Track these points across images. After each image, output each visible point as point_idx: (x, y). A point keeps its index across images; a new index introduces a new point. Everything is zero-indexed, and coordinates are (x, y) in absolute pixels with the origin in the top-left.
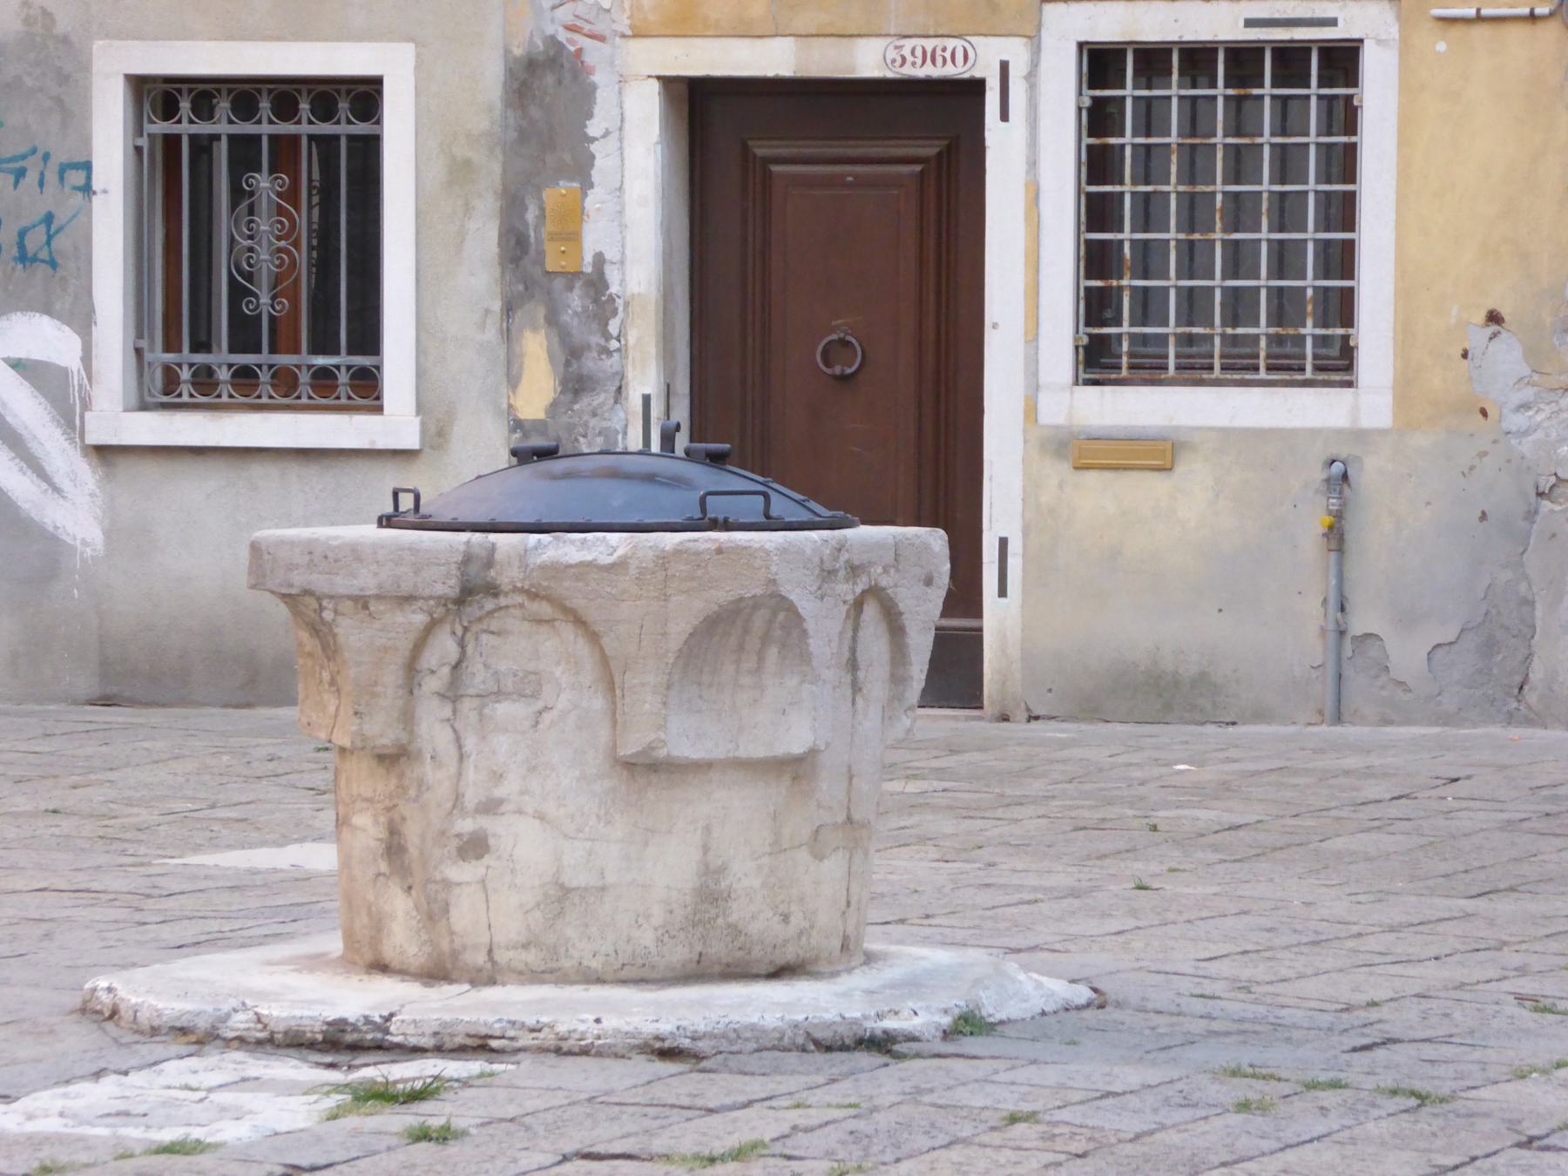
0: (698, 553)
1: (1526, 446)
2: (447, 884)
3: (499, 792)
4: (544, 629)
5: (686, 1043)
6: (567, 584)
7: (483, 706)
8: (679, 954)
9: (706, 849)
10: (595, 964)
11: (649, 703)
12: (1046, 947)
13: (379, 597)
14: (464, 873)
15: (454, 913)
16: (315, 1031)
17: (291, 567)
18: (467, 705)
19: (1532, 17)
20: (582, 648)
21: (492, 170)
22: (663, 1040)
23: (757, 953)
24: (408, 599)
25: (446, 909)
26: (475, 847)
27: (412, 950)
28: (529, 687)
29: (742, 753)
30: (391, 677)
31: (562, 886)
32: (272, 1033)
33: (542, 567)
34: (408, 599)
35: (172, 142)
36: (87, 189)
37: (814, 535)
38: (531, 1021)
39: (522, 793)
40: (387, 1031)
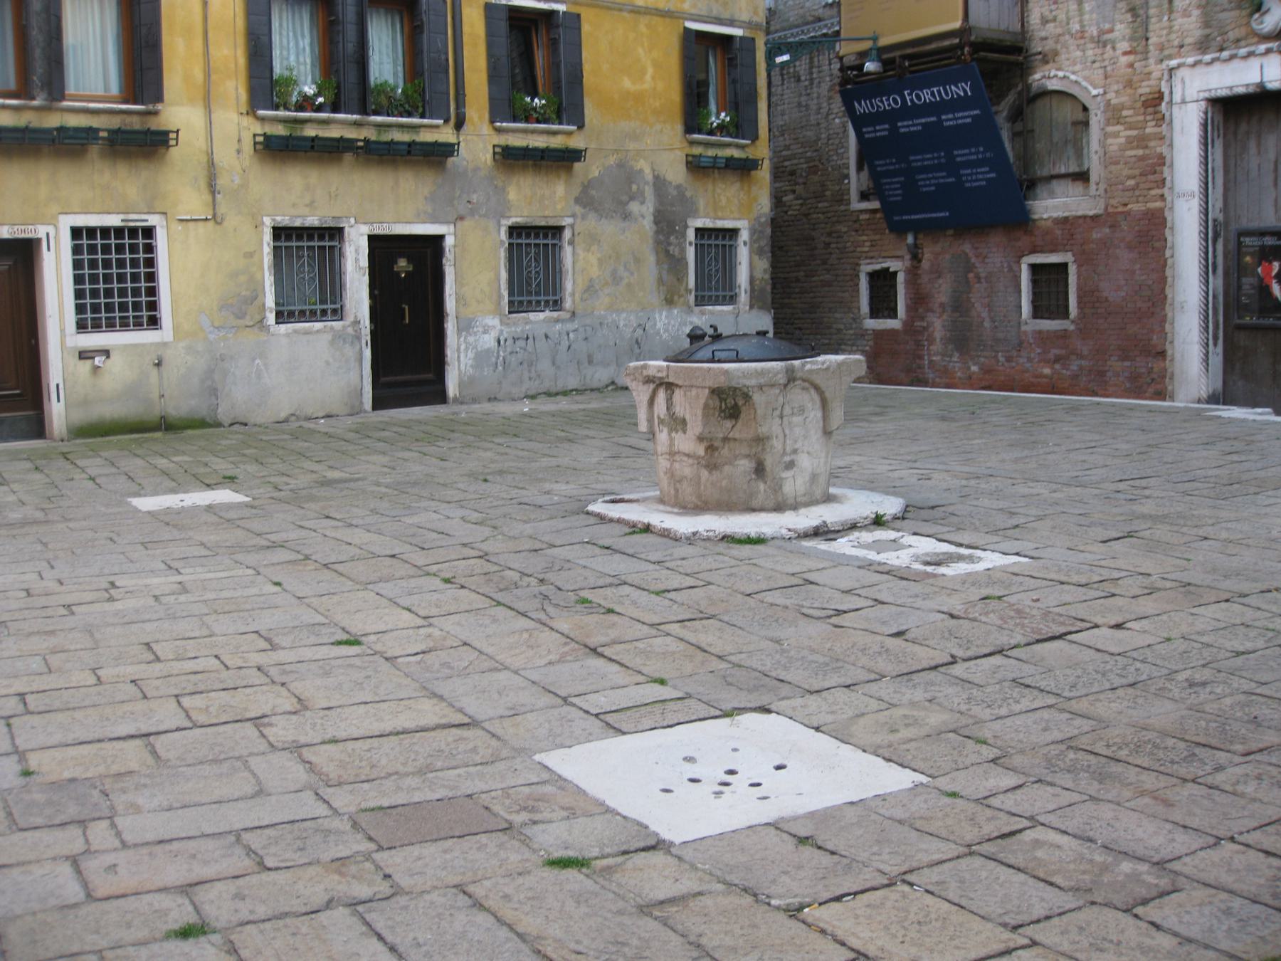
2: (782, 479)
3: (796, 447)
12: (336, 523)
15: (784, 488)
17: (739, 377)
19: (206, 219)
25: (781, 487)
37: (774, 363)
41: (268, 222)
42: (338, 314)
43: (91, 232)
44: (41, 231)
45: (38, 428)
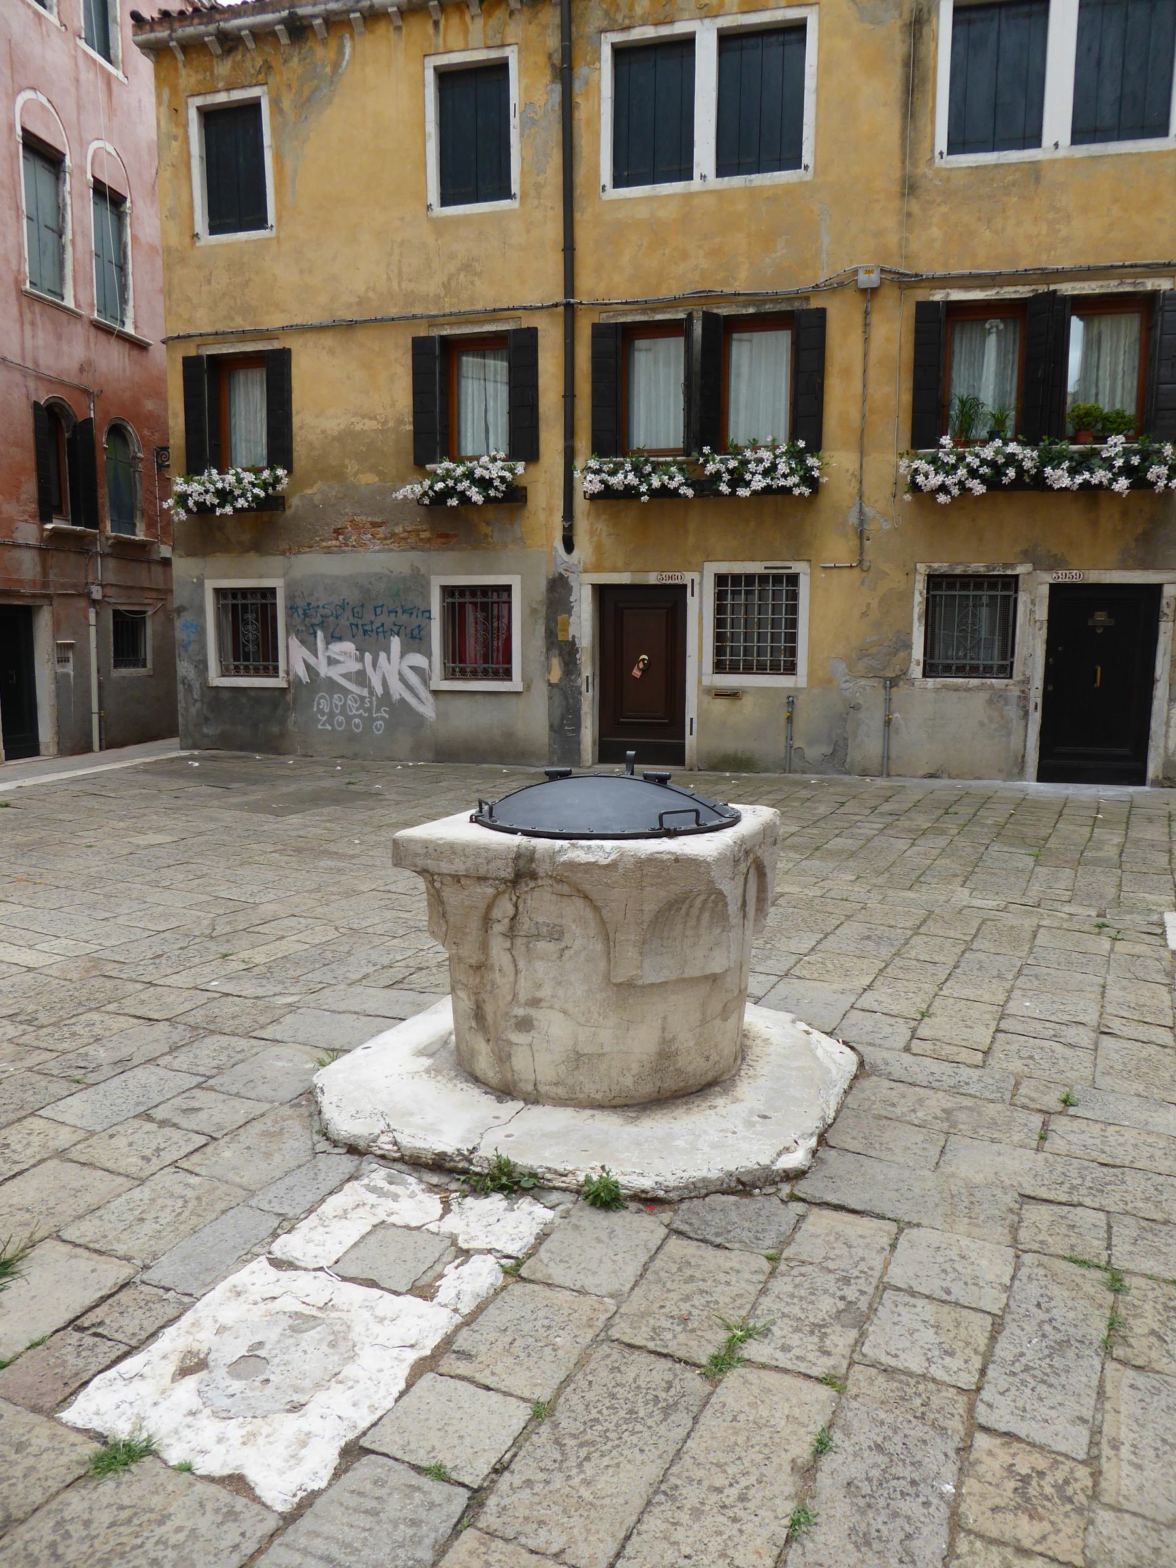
0: (662, 861)
1: (847, 693)
2: (510, 1043)
3: (539, 995)
4: (565, 899)
5: (661, 1193)
6: (579, 875)
7: (529, 943)
8: (647, 1089)
9: (664, 1029)
10: (599, 1096)
11: (632, 953)
13: (466, 876)
14: (516, 1037)
16: (428, 1158)
17: (417, 855)
18: (519, 942)
19: (851, 567)
20: (589, 914)
21: (543, 611)
22: (647, 1193)
23: (691, 1082)
24: (482, 879)
25: (509, 1056)
26: (525, 1025)
27: (491, 1074)
28: (556, 934)
29: (686, 976)
30: (474, 924)
31: (577, 1053)
32: (403, 1155)
33: (564, 863)
34: (482, 879)
35: (453, 604)
36: (430, 618)
38: (560, 1168)
39: (553, 997)
40: (470, 1162)
41: (922, 568)
42: (1006, 671)
43: (736, 579)
44: (687, 577)
45: (676, 756)
